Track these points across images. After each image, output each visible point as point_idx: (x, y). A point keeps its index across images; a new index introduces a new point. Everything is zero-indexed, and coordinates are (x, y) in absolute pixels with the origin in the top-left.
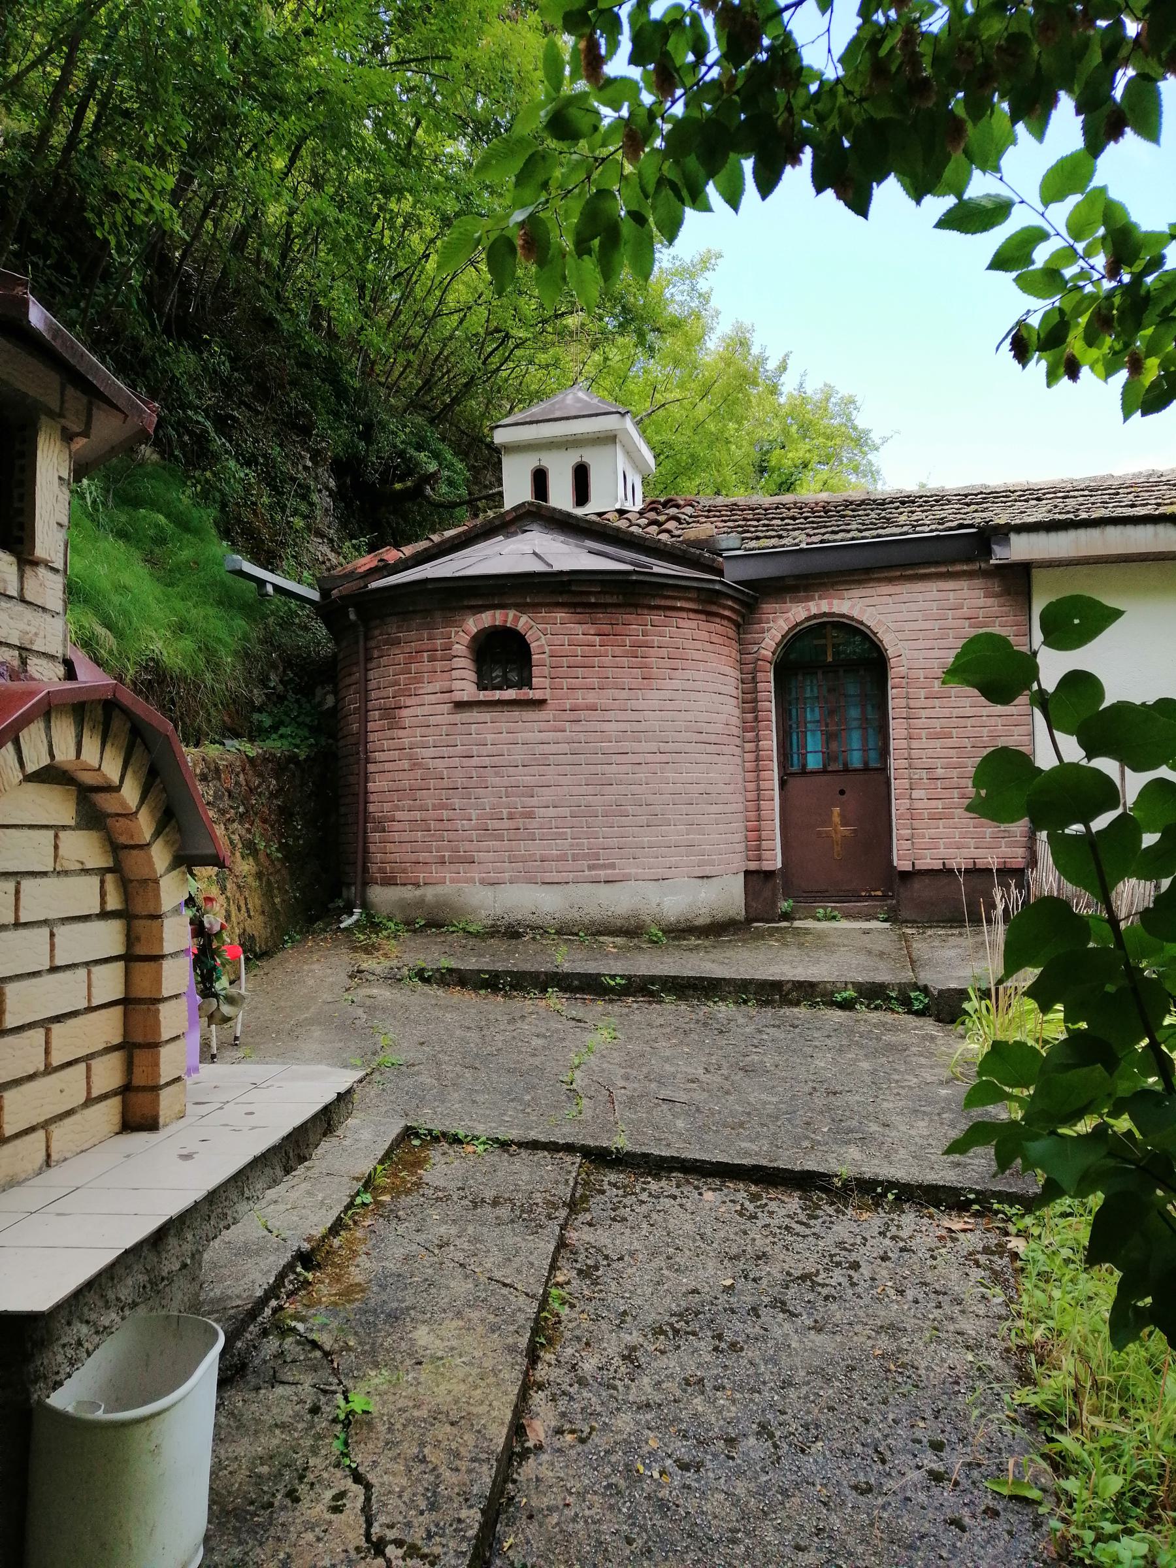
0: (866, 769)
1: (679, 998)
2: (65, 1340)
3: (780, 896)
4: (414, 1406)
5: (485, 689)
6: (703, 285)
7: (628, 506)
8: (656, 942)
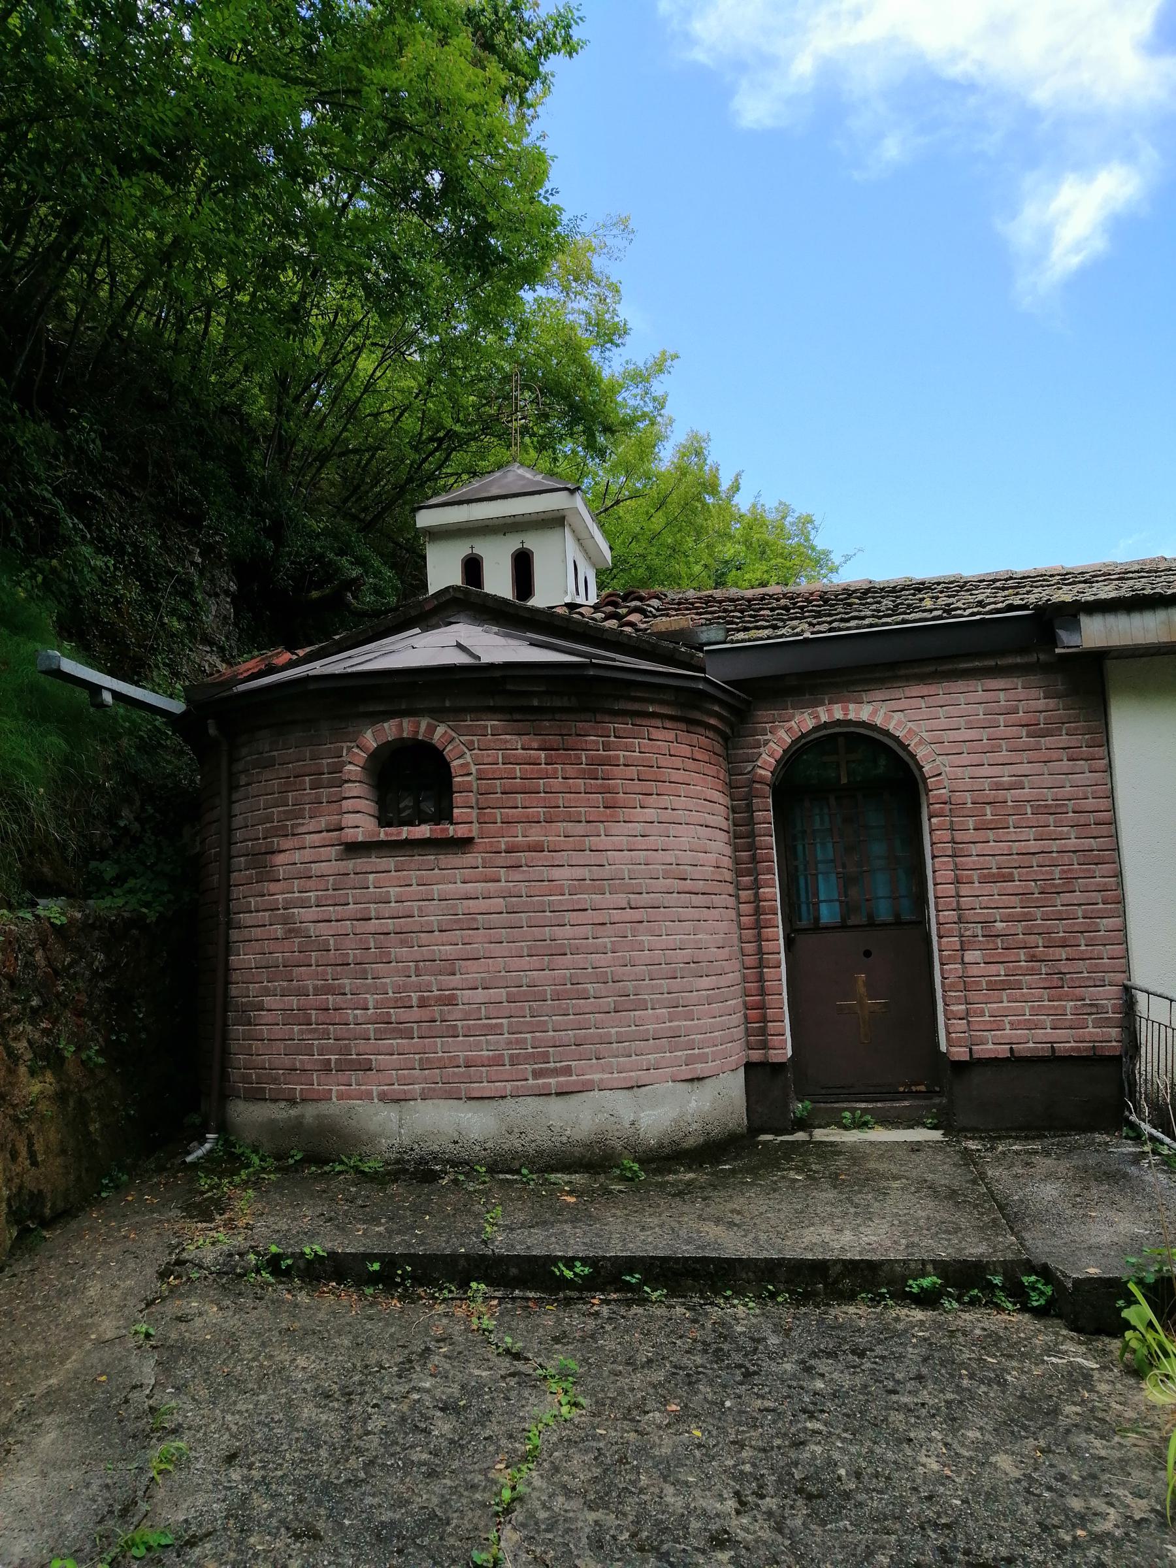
0: (898, 923)
1: (672, 1294)
3: (792, 1095)
5: (390, 825)
6: (658, 387)
7: (580, 600)
8: (631, 1179)
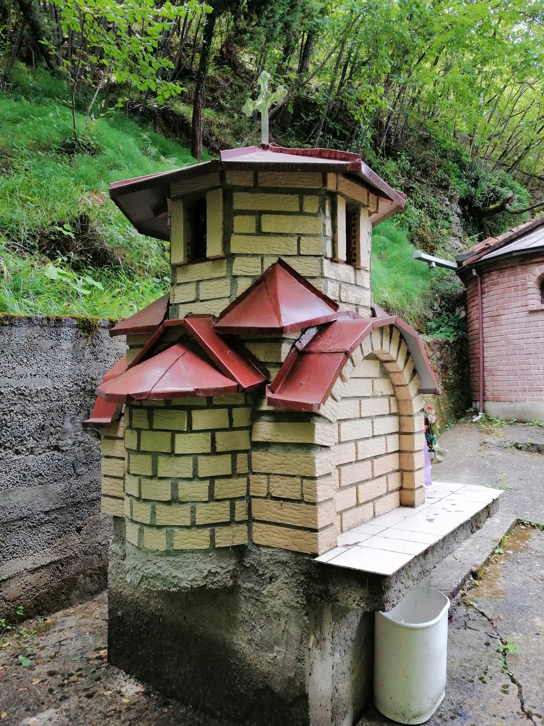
2: (395, 588)
4: (538, 655)
